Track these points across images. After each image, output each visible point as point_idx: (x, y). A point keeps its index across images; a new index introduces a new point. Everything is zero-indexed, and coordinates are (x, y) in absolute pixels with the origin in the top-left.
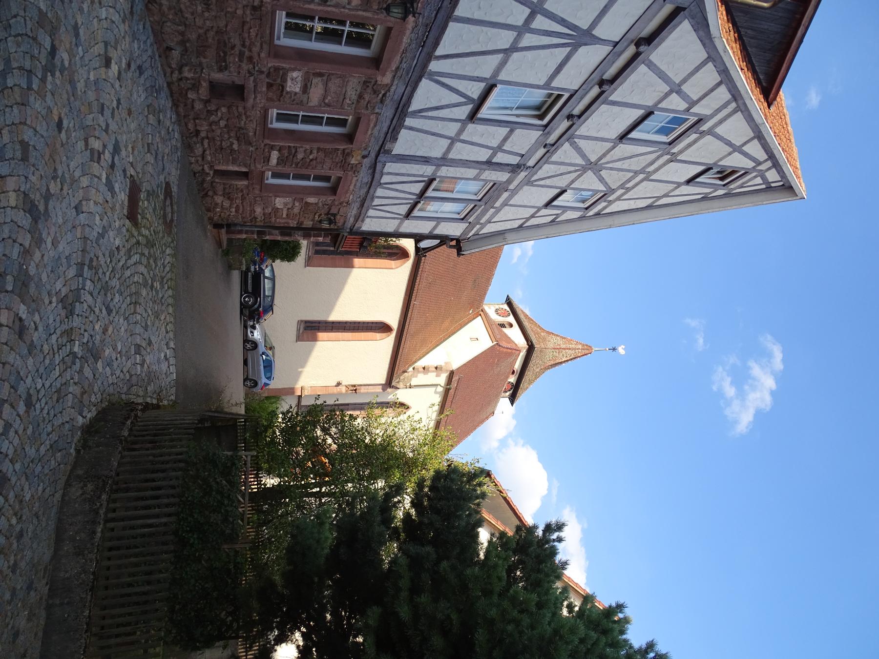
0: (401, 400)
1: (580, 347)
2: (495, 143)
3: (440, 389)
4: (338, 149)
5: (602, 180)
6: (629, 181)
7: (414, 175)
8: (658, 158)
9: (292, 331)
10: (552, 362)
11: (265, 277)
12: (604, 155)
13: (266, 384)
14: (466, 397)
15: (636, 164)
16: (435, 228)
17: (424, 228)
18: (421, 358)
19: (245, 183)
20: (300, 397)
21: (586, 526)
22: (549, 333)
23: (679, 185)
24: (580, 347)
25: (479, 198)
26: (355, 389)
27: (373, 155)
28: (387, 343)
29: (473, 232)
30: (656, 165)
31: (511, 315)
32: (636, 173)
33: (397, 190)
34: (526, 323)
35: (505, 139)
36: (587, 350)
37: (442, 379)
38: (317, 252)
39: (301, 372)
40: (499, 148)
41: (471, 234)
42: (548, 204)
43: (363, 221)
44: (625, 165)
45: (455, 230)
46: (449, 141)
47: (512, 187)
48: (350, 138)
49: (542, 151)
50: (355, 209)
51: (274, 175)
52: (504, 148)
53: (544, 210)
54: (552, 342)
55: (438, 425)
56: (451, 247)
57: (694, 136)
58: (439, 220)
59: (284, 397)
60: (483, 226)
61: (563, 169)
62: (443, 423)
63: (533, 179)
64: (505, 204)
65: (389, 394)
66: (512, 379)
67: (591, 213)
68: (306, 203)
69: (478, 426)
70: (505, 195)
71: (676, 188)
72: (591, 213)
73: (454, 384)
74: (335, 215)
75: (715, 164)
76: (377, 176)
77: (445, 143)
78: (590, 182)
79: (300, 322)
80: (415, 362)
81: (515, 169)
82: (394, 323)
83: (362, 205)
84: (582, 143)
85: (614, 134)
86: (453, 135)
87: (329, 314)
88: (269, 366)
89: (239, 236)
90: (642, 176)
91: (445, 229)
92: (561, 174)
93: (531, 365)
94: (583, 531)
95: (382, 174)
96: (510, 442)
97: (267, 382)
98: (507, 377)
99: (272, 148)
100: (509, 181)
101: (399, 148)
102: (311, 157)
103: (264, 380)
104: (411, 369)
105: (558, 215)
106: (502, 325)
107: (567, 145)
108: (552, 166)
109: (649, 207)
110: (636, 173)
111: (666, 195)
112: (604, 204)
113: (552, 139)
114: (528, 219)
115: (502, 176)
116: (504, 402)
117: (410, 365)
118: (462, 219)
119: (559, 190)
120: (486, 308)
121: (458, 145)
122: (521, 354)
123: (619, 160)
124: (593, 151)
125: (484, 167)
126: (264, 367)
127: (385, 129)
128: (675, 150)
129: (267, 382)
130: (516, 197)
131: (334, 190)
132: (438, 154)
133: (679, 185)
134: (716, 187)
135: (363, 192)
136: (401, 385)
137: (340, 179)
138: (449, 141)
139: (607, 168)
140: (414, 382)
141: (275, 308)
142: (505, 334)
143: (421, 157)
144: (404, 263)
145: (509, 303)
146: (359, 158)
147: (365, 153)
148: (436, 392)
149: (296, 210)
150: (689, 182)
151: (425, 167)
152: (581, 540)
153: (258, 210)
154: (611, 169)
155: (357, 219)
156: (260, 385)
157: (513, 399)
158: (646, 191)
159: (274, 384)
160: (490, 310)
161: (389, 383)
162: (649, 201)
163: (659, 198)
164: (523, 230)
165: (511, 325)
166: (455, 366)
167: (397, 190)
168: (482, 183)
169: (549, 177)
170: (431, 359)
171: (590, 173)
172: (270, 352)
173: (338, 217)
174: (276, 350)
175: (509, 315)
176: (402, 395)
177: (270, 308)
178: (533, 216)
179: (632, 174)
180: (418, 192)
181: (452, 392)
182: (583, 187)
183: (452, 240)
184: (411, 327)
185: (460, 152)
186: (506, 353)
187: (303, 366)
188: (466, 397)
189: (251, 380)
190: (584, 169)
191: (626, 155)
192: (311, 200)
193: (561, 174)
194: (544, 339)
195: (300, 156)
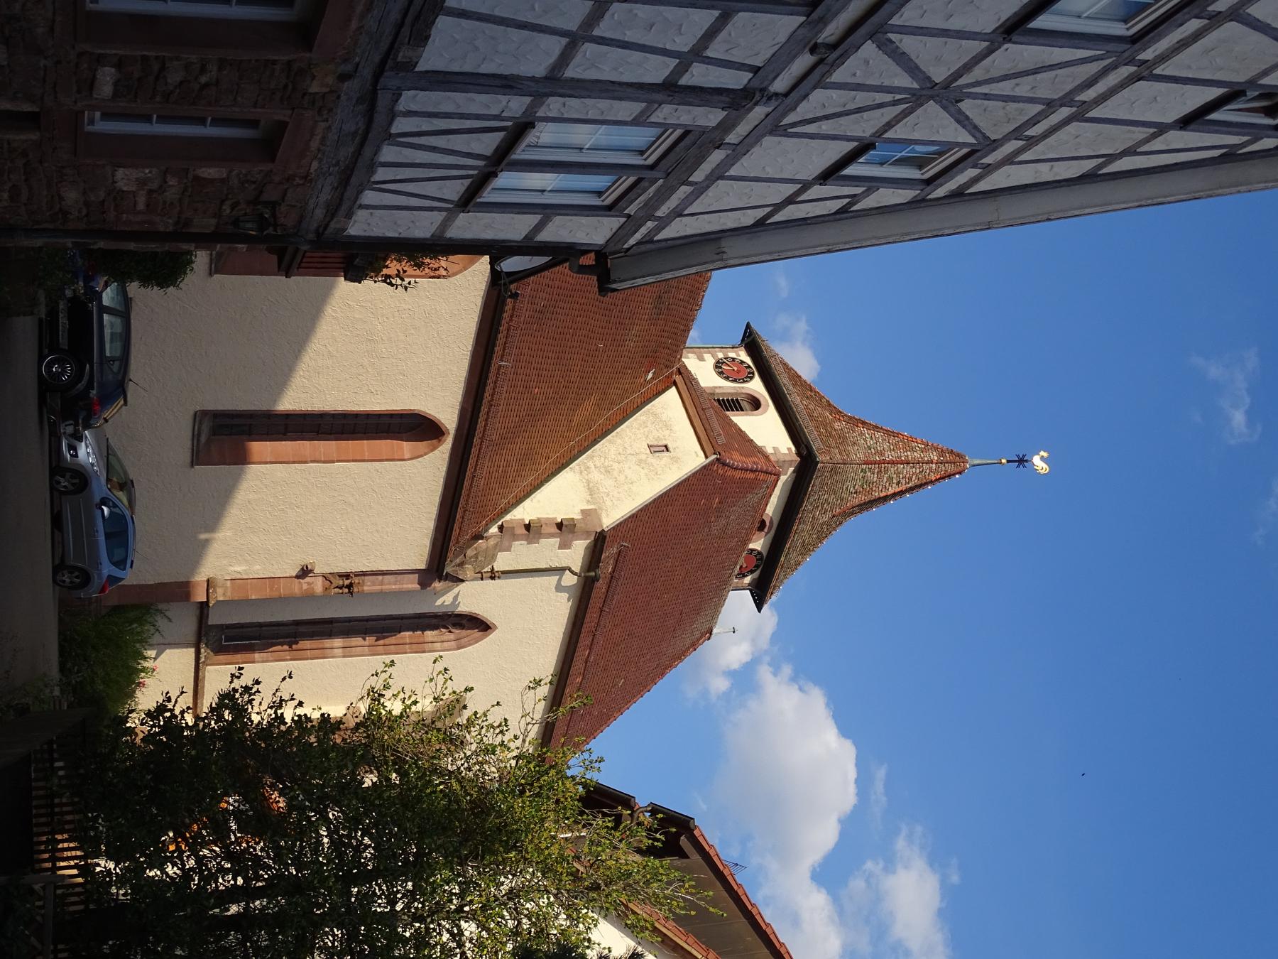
0: (463, 608)
2: (683, 43)
3: (570, 580)
4: (274, 62)
5: (963, 120)
6: (1034, 121)
7: (478, 117)
8: (1105, 72)
9: (177, 437)
10: (863, 498)
11: (103, 309)
12: (967, 68)
13: (113, 580)
14: (637, 601)
15: (1047, 87)
16: (539, 228)
17: (514, 228)
18: (519, 501)
19: (34, 136)
20: (204, 606)
21: (955, 879)
22: (855, 422)
23: (1161, 129)
25: (650, 161)
26: (347, 582)
27: (367, 72)
28: (425, 471)
29: (638, 236)
30: (1101, 87)
31: (757, 378)
32: (1051, 105)
33: (434, 149)
34: (795, 399)
35: (711, 34)
36: (953, 463)
37: (575, 555)
39: (207, 541)
40: (697, 54)
41: (632, 241)
42: (828, 175)
43: (349, 215)
44: (1023, 88)
45: (593, 232)
46: (564, 41)
47: (732, 138)
48: (304, 33)
49: (804, 61)
50: (327, 189)
51: (107, 116)
52: (709, 53)
53: (817, 187)
54: (864, 444)
55: (548, 732)
56: (583, 269)
57: (1194, 25)
58: (548, 211)
59: (160, 606)
60: (664, 222)
61: (862, 98)
62: (559, 729)
63: (786, 121)
64: (718, 175)
65: (438, 594)
66: (758, 544)
67: (940, 192)
68: (197, 178)
69: (670, 665)
70: (717, 156)
71: (1154, 136)
72: (940, 192)
73: (607, 567)
74: (273, 205)
75: (1252, 83)
76: (380, 118)
77: (555, 46)
78: (932, 126)
79: (201, 416)
80: (506, 511)
81: (738, 100)
82: (448, 417)
83: (345, 180)
84: (907, 43)
85: (989, 21)
86: (573, 26)
88: (119, 532)
89: (26, 242)
90: (1065, 112)
91: (560, 230)
92: (859, 110)
93: (807, 505)
94: (947, 890)
95: (392, 116)
96: (765, 673)
97: (117, 572)
98: (747, 540)
99: (100, 60)
100: (726, 127)
101: (433, 58)
102: (203, 79)
103: (107, 569)
104: (494, 530)
105: (854, 198)
106: (733, 404)
107: (869, 49)
108: (834, 94)
109: (1089, 178)
110: (1051, 105)
111: (1130, 152)
112: (972, 173)
113: (831, 32)
114: (778, 208)
115: (710, 117)
116: (739, 602)
117: (493, 521)
118: (609, 208)
119: (852, 145)
120: (690, 362)
121: (589, 49)
122: (783, 478)
123: (1006, 77)
124: (938, 59)
125: (658, 97)
126: (108, 536)
127: (395, 16)
128: (1148, 55)
129: (117, 572)
130: (745, 161)
131: (269, 145)
132: (540, 70)
133: (1161, 129)
134: (1256, 132)
135: (346, 152)
136: (469, 571)
137: (282, 126)
138: (564, 41)
139: (975, 96)
141: (131, 389)
142: (741, 433)
143: (494, 76)
145: (751, 342)
146: (330, 80)
147: (348, 68)
148: (559, 588)
149: (171, 194)
150: (1186, 122)
151: (504, 99)
152: (941, 913)
153: (71, 196)
154: (986, 97)
155: (333, 210)
156: (96, 582)
157: (760, 595)
158: (1076, 145)
159: (140, 573)
160: (703, 370)
161: (438, 567)
162: (1088, 165)
163: (1111, 158)
164: (768, 234)
165: (756, 404)
166: (609, 520)
167: (434, 149)
168: (655, 131)
169: (827, 117)
171: (932, 107)
172: (122, 496)
173: (283, 208)
174: (138, 491)
175: (750, 377)
176: (469, 596)
177: (117, 390)
178: (790, 200)
179: (1039, 108)
180: (488, 151)
181: (601, 586)
182: (916, 136)
183: (586, 252)
184: (494, 425)
185: (592, 63)
186: (742, 481)
188: (637, 601)
189: (72, 569)
190: (916, 100)
191: (1022, 67)
192: (210, 172)
193: (859, 110)
194: (842, 438)
195: (174, 78)
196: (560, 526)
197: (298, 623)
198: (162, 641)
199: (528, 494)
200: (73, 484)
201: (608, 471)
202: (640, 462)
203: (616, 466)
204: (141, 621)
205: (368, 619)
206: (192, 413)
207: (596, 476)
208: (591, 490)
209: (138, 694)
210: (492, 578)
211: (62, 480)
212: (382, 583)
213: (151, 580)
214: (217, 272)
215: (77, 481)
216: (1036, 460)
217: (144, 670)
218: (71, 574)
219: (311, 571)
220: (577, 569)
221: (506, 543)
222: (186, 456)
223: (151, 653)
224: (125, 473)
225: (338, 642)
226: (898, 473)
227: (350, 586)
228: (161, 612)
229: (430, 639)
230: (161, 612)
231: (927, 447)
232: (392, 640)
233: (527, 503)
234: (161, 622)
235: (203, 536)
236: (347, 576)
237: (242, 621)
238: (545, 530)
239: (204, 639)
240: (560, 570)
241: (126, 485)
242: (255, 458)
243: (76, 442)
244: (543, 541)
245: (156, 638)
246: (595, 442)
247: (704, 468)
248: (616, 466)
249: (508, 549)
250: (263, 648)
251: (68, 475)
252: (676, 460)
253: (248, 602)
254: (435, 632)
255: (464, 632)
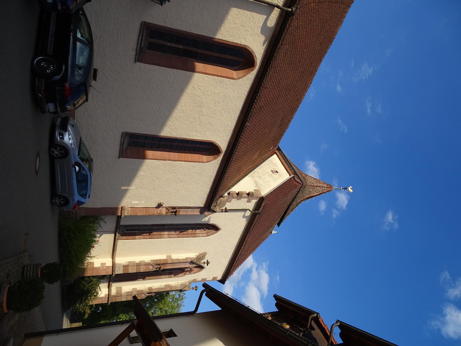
0: (211, 222)
1: (325, 185)
3: (248, 214)
10: (308, 196)
11: (76, 39)
13: (80, 203)
24: (325, 185)
26: (174, 211)
28: (212, 166)
37: (251, 205)
38: (151, 46)
59: (103, 217)
79: (105, 263)
80: (230, 188)
87: (215, 34)
88: (84, 182)
97: (83, 200)
103: (77, 197)
104: (226, 194)
117: (226, 191)
136: (217, 209)
140: (228, 206)
144: (248, 73)
148: (244, 217)
156: (71, 205)
159: (91, 203)
161: (209, 206)
166: (264, 192)
170: (245, 185)
174: (96, 165)
176: (213, 218)
177: (82, 89)
187: (129, 183)
189: (60, 197)
196: (248, 194)
197: (153, 225)
198: (102, 230)
199: (236, 183)
200: (61, 154)
201: (260, 178)
202: (270, 175)
203: (262, 176)
204: (94, 222)
205: (177, 225)
206: (140, 22)
207: (257, 179)
208: (256, 183)
209: (92, 251)
210: (226, 211)
211: (55, 151)
212: (187, 212)
213: (98, 205)
214: (138, 62)
215: (63, 152)
216: (349, 188)
217: (95, 241)
218: (59, 198)
219: (162, 205)
220: (251, 210)
221: (230, 199)
222: (117, 153)
223: (98, 235)
224: (89, 155)
225: (166, 233)
226: (317, 189)
227: (176, 211)
228: (102, 219)
229: (198, 233)
230: (102, 219)
231: (324, 183)
232: (185, 233)
233: (236, 186)
234: (102, 223)
235: (124, 188)
236: (174, 208)
237: (133, 224)
238: (243, 195)
239: (118, 231)
240: (245, 210)
241: (89, 161)
242: (197, 70)
243: (62, 132)
244: (242, 199)
245: (100, 229)
246: (255, 168)
247: (290, 179)
248: (262, 176)
249: (230, 202)
250: (140, 234)
251: (58, 148)
252: (280, 176)
253: (136, 217)
254: (200, 230)
255: (209, 231)
